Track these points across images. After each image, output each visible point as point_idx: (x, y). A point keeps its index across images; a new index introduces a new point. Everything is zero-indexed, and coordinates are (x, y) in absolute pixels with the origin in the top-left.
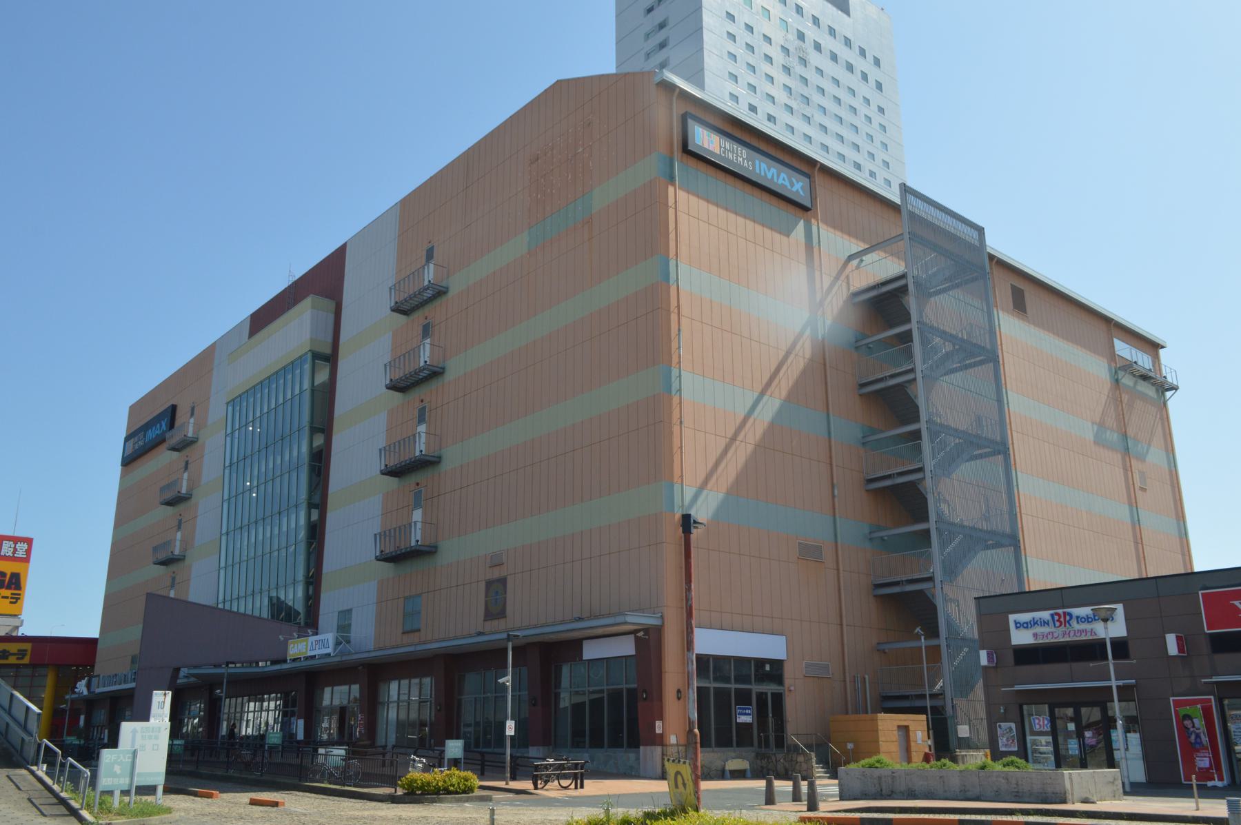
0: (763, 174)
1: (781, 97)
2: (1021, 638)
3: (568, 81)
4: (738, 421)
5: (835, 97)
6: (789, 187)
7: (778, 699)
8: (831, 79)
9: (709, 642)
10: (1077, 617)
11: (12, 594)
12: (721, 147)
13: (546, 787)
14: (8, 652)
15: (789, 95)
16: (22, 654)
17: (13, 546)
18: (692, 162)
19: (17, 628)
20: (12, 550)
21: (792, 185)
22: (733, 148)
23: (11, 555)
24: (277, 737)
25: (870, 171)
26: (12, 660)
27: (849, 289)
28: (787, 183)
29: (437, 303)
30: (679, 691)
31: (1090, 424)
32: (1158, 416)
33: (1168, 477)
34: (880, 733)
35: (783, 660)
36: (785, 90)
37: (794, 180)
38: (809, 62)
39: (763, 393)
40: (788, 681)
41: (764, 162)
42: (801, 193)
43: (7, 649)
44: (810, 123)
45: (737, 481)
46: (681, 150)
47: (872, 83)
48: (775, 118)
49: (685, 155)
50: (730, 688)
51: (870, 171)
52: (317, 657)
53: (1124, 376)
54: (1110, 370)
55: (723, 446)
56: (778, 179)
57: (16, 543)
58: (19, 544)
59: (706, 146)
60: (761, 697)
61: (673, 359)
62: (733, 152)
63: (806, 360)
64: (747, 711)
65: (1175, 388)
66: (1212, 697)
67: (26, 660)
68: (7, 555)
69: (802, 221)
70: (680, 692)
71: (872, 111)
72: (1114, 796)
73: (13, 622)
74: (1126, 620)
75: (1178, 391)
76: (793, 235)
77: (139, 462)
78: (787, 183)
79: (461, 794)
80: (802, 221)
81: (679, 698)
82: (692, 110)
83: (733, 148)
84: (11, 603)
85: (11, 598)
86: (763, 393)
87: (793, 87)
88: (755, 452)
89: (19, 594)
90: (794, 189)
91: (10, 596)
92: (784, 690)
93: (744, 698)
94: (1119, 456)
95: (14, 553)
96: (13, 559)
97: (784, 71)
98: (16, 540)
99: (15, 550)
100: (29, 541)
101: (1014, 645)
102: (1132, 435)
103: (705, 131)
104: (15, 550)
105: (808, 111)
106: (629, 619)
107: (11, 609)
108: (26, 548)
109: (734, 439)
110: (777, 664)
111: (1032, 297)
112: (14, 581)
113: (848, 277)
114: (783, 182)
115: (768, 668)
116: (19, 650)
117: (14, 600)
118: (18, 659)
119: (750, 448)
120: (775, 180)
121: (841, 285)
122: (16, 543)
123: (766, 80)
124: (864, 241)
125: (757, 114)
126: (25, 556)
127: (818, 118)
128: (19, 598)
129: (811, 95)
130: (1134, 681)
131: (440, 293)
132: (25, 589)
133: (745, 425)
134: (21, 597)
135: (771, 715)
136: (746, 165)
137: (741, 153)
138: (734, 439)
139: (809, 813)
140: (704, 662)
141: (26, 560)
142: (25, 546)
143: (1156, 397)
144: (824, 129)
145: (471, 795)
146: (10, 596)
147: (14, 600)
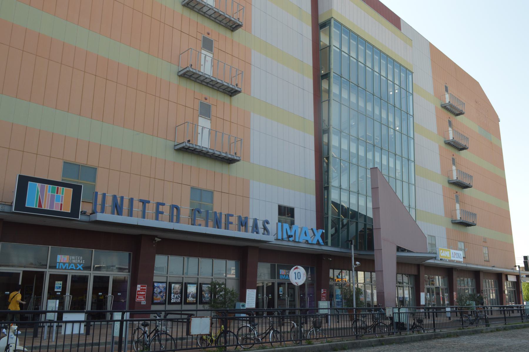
12: (70, 259)
22: (76, 258)
137: (80, 259)
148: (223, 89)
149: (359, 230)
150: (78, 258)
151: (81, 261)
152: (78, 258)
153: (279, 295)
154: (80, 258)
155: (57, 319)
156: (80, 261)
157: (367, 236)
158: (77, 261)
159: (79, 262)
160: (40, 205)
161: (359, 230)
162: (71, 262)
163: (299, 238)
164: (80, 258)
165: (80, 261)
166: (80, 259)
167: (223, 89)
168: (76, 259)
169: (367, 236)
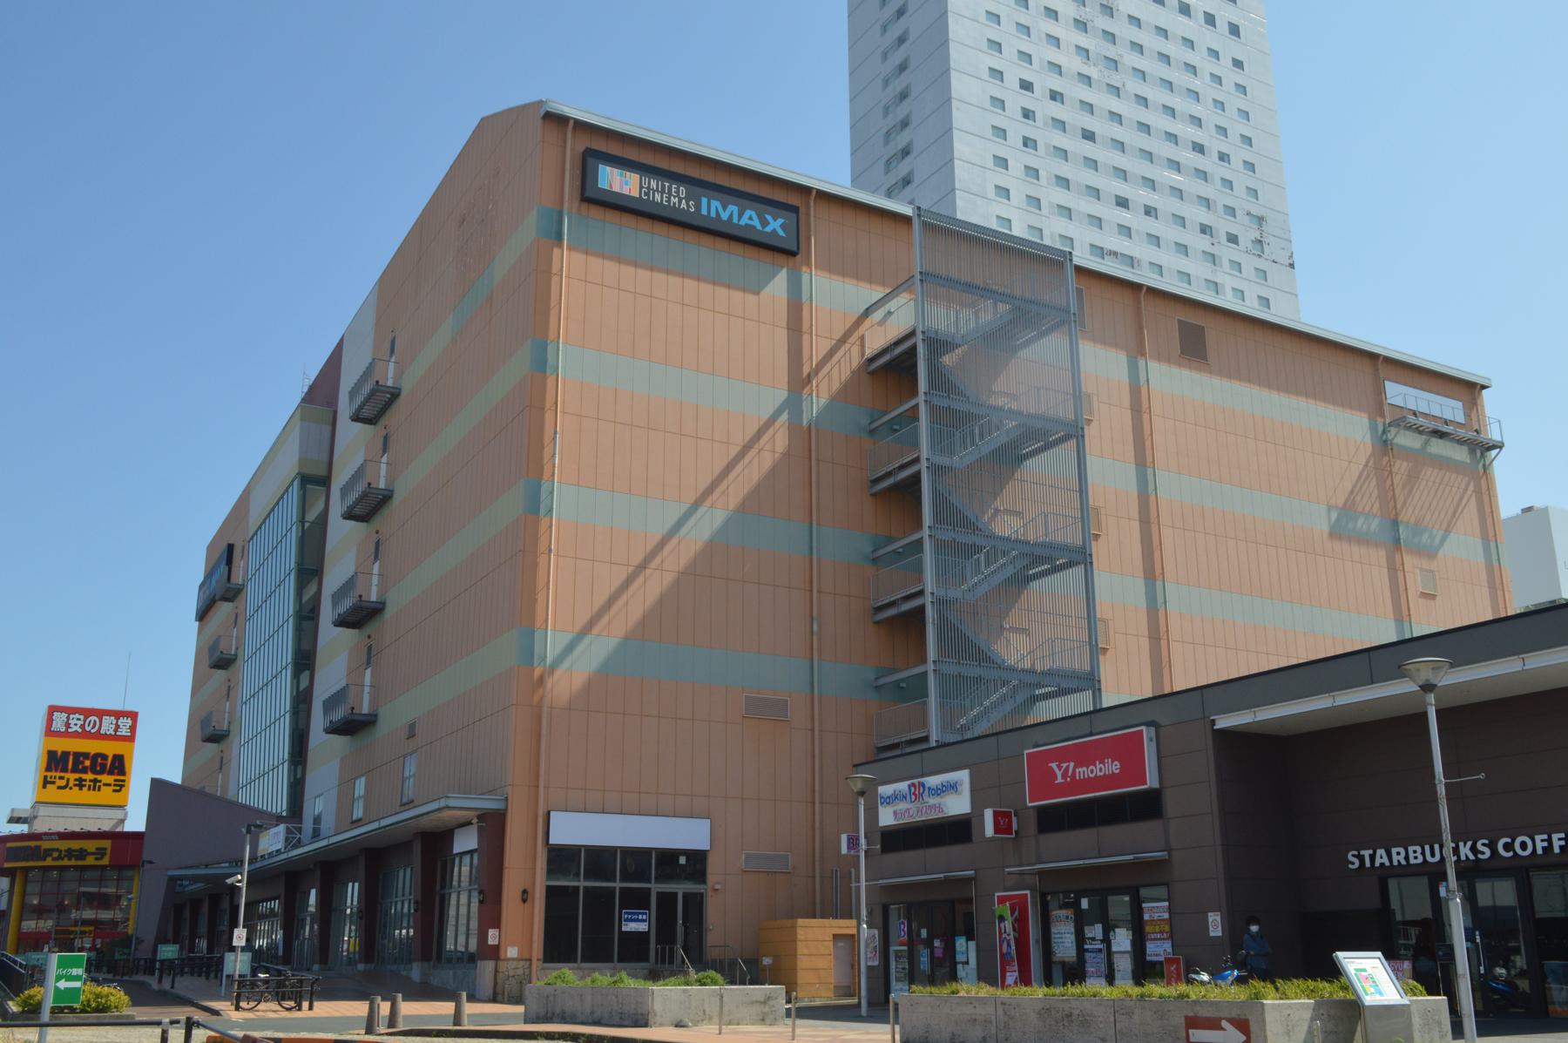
0: (713, 214)
1: (1072, 63)
2: (886, 818)
3: (488, 117)
4: (651, 544)
5: (1160, 54)
6: (759, 227)
7: (695, 904)
8: (1154, 30)
9: (570, 829)
10: (929, 788)
11: (115, 780)
12: (641, 187)
13: (259, 1007)
14: (86, 850)
15: (1084, 60)
16: (100, 853)
17: (114, 722)
18: (596, 212)
19: (122, 821)
20: (114, 727)
21: (765, 223)
22: (663, 186)
23: (113, 733)
24: (172, 951)
25: (1219, 152)
26: (90, 861)
27: (863, 354)
28: (756, 223)
29: (394, 407)
30: (525, 892)
31: (1323, 508)
32: (1471, 488)
33: (1484, 576)
34: (799, 945)
35: (708, 851)
36: (1078, 54)
37: (769, 218)
38: (1118, 10)
39: (697, 504)
40: (712, 878)
41: (714, 199)
42: (781, 233)
43: (85, 848)
44: (1119, 97)
45: (644, 622)
46: (577, 194)
47: (1222, 26)
48: (1062, 95)
49: (584, 205)
50: (615, 888)
51: (1219, 152)
52: (266, 857)
53: (1397, 433)
54: (1373, 427)
55: (623, 577)
56: (739, 220)
57: (117, 719)
58: (121, 720)
59: (616, 189)
60: (667, 900)
61: (545, 470)
62: (663, 192)
63: (777, 455)
64: (640, 917)
65: (1499, 446)
66: (1028, 892)
67: (105, 861)
68: (108, 733)
69: (784, 271)
70: (527, 893)
71: (1224, 68)
72: (763, 1020)
73: (118, 814)
74: (972, 791)
75: (1504, 448)
76: (768, 290)
77: (210, 613)
78: (756, 223)
79: (89, 1012)
80: (784, 271)
81: (524, 901)
82: (600, 145)
83: (663, 186)
84: (114, 791)
85: (115, 785)
86: (697, 504)
87: (1091, 48)
88: (677, 583)
89: (124, 781)
90: (768, 229)
91: (113, 783)
92: (706, 890)
93: (636, 901)
94: (1382, 553)
95: (116, 731)
96: (115, 737)
97: (1077, 28)
98: (118, 714)
99: (117, 727)
100: (133, 716)
101: (882, 827)
102: (1412, 521)
103: (616, 170)
104: (117, 727)
105: (1116, 80)
106: (452, 803)
107: (115, 798)
108: (130, 724)
109: (643, 566)
110: (697, 859)
111: (1215, 334)
112: (117, 764)
113: (862, 338)
114: (750, 222)
115: (682, 860)
116: (97, 849)
117: (118, 788)
118: (96, 859)
119: (669, 578)
120: (735, 220)
121: (849, 349)
122: (117, 719)
123: (1048, 43)
124: (884, 285)
125: (1243, 70)
126: (129, 734)
127: (1134, 86)
128: (123, 786)
129: (1120, 55)
130: (973, 872)
131: (395, 395)
132: (130, 773)
133: (662, 548)
134: (126, 783)
135: (681, 922)
136: (684, 205)
137: (678, 192)
138: (643, 566)
139: (366, 1036)
140: (561, 858)
141: (131, 739)
142: (129, 721)
143: (1468, 460)
144: (1143, 101)
145: (109, 1014)
146: (113, 783)
147: (118, 788)
148: (761, 1003)
149: (301, 688)
150: (670, 188)
151: (684, 201)
152: (670, 188)
153: (1001, 954)
154: (678, 189)
155: (850, 917)
156: (680, 202)
157: (1300, 1001)
158: (669, 198)
159: (674, 204)
160: (611, 187)
161: (301, 688)
162: (649, 197)
163: (1403, 913)
164: (678, 189)
165: (680, 202)
166: (678, 192)
167: (761, 1003)
168: (663, 192)
169: (1300, 1001)
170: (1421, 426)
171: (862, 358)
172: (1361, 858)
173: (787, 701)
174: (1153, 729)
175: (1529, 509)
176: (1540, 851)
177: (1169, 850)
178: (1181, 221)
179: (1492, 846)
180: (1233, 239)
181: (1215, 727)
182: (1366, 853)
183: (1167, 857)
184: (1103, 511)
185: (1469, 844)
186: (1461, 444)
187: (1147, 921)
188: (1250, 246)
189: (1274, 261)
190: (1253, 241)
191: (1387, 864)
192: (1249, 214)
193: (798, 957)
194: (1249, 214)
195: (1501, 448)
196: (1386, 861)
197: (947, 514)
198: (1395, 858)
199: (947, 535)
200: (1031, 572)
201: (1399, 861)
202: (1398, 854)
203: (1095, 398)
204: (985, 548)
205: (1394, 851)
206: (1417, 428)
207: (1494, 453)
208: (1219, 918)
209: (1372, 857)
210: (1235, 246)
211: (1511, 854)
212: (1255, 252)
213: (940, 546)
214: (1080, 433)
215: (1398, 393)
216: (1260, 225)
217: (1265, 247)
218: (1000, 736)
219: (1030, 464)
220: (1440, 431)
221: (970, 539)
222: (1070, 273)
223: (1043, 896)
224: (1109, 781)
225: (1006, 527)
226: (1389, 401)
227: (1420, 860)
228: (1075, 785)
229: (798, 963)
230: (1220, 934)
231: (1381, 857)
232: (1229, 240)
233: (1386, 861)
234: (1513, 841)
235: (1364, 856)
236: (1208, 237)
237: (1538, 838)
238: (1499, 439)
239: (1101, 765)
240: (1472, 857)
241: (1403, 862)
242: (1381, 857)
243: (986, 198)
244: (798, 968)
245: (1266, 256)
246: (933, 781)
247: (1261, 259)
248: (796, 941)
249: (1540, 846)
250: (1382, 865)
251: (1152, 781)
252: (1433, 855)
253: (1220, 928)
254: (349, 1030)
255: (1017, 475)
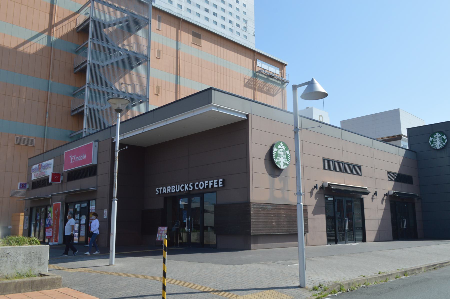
66: (60, 202)
74: (54, 167)
75: (289, 83)
170: (266, 74)
171: (76, 27)
172: (159, 190)
173: (34, 140)
174: (97, 143)
175: (308, 108)
176: (205, 187)
177: (97, 187)
178: (223, 18)
179: (193, 185)
180: (238, 25)
181: (113, 141)
182: (161, 188)
183: (96, 190)
184: (160, 88)
185: (188, 184)
186: (278, 81)
187: (90, 213)
188: (243, 28)
189: (249, 33)
190: (244, 27)
191: (166, 192)
192: (243, 19)
193: (20, 226)
194: (243, 19)
195: (288, 82)
196: (165, 191)
197: (96, 78)
198: (168, 190)
199: (95, 87)
200: (132, 104)
201: (169, 191)
202: (169, 189)
203: (161, 51)
204: (114, 94)
205: (168, 187)
206: (265, 74)
207: (286, 84)
208: (106, 212)
209: (162, 190)
210: (239, 28)
211: (198, 188)
212: (244, 30)
213: (91, 91)
214: (149, 59)
215: (261, 64)
216: (246, 23)
217: (247, 29)
218: (62, 147)
219: (135, 69)
220: (271, 76)
221: (107, 90)
222: (150, 8)
223: (67, 204)
224: (83, 161)
225: (117, 86)
226: (257, 65)
227: (174, 191)
228: (76, 163)
229: (20, 228)
230: (106, 217)
231: (164, 190)
232: (237, 26)
233: (165, 191)
234: (199, 183)
235: (160, 189)
236: (231, 24)
237: (206, 182)
238: (288, 80)
239: (82, 156)
240: (188, 190)
241: (170, 192)
242: (164, 190)
243: (165, 3)
244: (19, 229)
245: (247, 32)
246: (45, 163)
247: (246, 33)
248: (19, 220)
249: (206, 185)
250: (164, 192)
251: (94, 161)
252: (178, 189)
253: (106, 215)
254: (181, 238)
255: (131, 72)
